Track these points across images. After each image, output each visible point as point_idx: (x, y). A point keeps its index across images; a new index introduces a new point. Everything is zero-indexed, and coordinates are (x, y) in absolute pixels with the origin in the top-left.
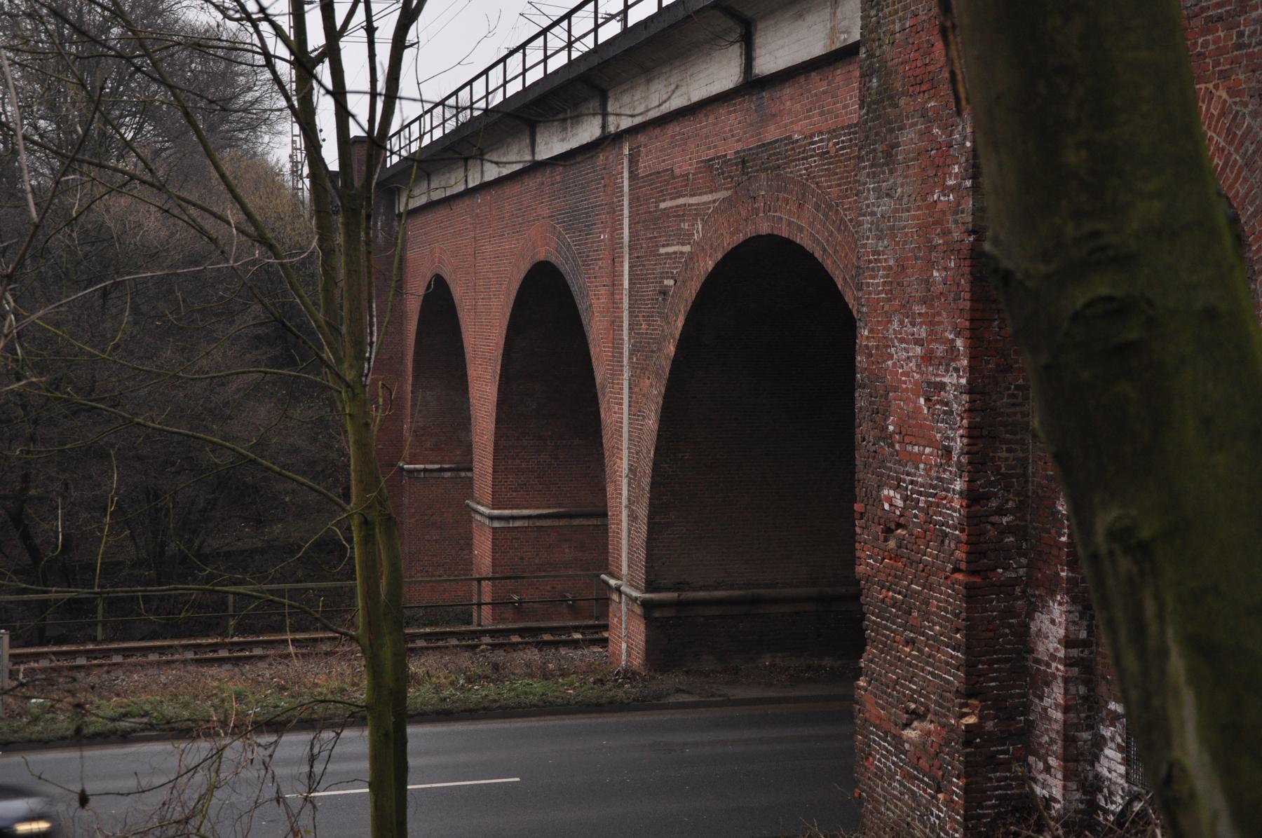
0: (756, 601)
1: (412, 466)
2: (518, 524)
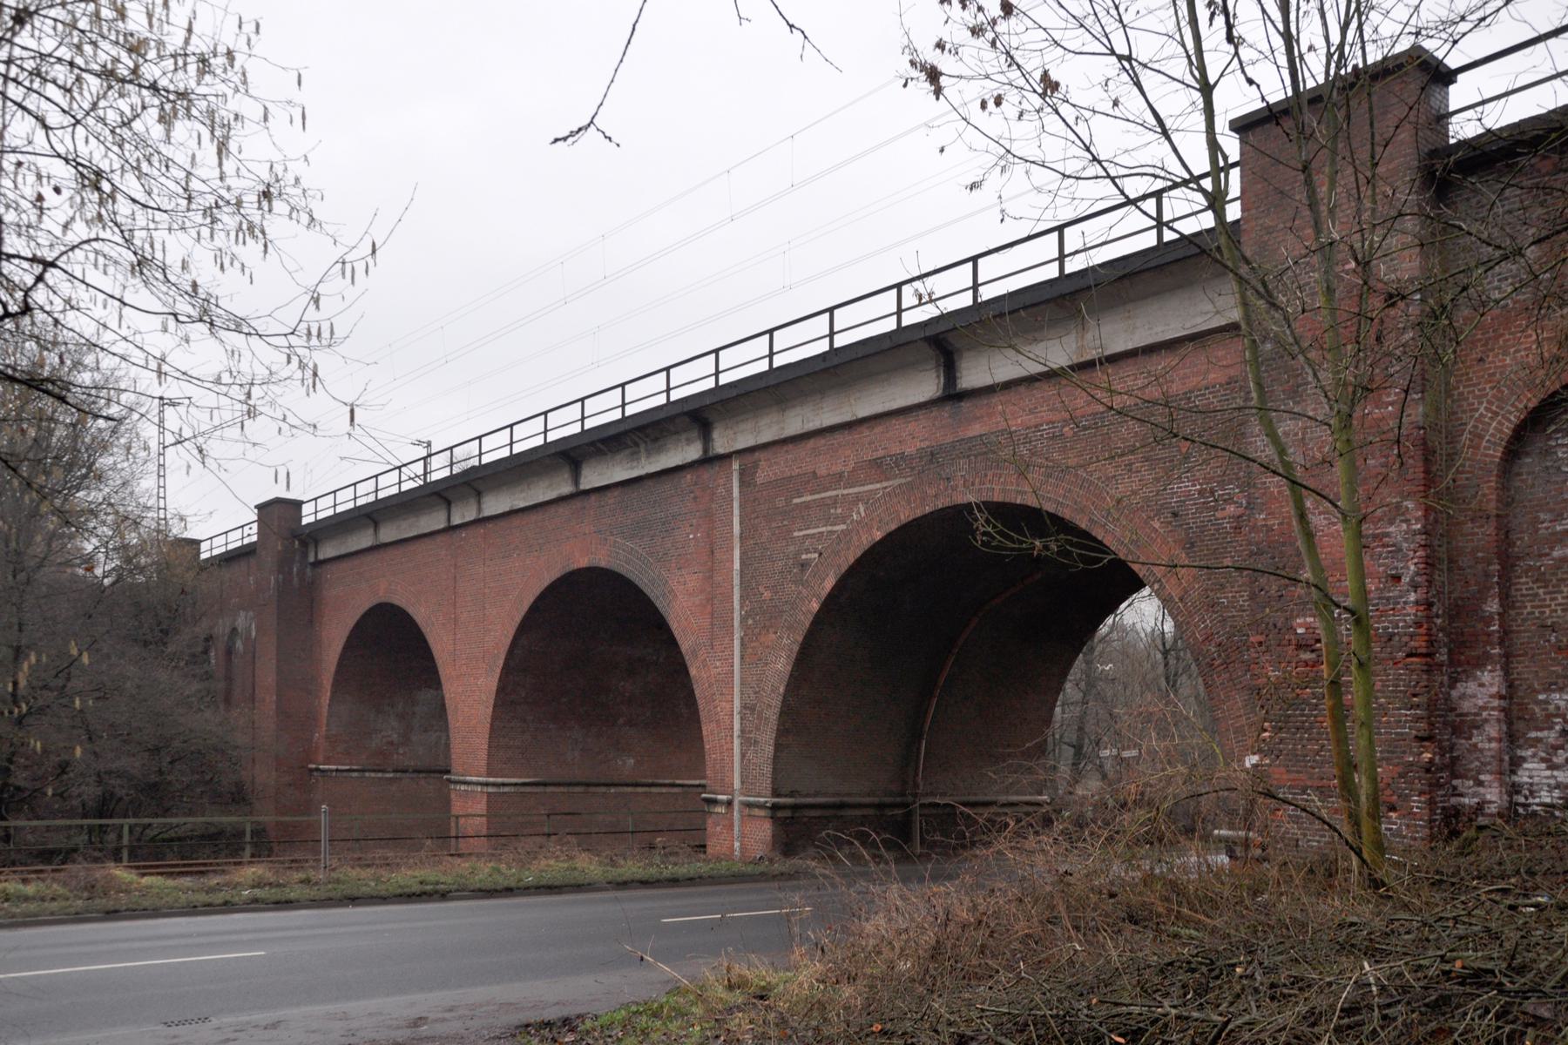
0: (842, 806)
2: (506, 789)
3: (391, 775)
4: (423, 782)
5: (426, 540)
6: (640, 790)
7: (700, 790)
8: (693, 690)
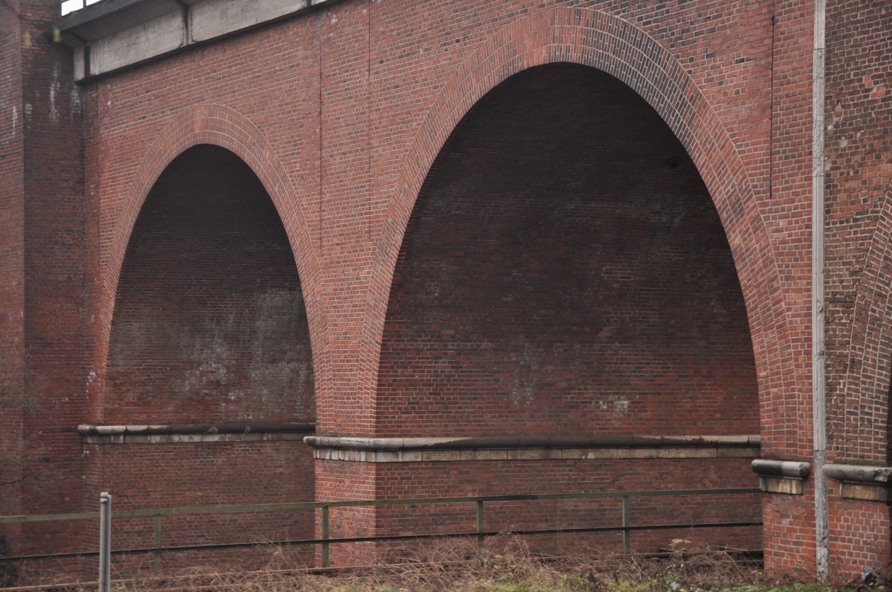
1: (109, 428)
2: (409, 457)
3: (216, 438)
4: (268, 449)
5: (274, 35)
6: (640, 453)
7: (749, 452)
8: (734, 274)
